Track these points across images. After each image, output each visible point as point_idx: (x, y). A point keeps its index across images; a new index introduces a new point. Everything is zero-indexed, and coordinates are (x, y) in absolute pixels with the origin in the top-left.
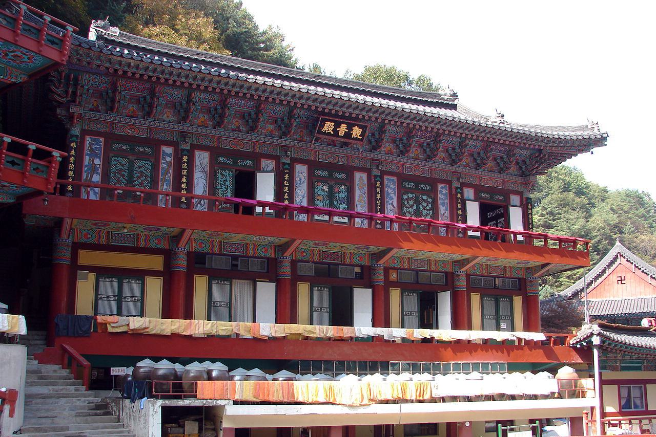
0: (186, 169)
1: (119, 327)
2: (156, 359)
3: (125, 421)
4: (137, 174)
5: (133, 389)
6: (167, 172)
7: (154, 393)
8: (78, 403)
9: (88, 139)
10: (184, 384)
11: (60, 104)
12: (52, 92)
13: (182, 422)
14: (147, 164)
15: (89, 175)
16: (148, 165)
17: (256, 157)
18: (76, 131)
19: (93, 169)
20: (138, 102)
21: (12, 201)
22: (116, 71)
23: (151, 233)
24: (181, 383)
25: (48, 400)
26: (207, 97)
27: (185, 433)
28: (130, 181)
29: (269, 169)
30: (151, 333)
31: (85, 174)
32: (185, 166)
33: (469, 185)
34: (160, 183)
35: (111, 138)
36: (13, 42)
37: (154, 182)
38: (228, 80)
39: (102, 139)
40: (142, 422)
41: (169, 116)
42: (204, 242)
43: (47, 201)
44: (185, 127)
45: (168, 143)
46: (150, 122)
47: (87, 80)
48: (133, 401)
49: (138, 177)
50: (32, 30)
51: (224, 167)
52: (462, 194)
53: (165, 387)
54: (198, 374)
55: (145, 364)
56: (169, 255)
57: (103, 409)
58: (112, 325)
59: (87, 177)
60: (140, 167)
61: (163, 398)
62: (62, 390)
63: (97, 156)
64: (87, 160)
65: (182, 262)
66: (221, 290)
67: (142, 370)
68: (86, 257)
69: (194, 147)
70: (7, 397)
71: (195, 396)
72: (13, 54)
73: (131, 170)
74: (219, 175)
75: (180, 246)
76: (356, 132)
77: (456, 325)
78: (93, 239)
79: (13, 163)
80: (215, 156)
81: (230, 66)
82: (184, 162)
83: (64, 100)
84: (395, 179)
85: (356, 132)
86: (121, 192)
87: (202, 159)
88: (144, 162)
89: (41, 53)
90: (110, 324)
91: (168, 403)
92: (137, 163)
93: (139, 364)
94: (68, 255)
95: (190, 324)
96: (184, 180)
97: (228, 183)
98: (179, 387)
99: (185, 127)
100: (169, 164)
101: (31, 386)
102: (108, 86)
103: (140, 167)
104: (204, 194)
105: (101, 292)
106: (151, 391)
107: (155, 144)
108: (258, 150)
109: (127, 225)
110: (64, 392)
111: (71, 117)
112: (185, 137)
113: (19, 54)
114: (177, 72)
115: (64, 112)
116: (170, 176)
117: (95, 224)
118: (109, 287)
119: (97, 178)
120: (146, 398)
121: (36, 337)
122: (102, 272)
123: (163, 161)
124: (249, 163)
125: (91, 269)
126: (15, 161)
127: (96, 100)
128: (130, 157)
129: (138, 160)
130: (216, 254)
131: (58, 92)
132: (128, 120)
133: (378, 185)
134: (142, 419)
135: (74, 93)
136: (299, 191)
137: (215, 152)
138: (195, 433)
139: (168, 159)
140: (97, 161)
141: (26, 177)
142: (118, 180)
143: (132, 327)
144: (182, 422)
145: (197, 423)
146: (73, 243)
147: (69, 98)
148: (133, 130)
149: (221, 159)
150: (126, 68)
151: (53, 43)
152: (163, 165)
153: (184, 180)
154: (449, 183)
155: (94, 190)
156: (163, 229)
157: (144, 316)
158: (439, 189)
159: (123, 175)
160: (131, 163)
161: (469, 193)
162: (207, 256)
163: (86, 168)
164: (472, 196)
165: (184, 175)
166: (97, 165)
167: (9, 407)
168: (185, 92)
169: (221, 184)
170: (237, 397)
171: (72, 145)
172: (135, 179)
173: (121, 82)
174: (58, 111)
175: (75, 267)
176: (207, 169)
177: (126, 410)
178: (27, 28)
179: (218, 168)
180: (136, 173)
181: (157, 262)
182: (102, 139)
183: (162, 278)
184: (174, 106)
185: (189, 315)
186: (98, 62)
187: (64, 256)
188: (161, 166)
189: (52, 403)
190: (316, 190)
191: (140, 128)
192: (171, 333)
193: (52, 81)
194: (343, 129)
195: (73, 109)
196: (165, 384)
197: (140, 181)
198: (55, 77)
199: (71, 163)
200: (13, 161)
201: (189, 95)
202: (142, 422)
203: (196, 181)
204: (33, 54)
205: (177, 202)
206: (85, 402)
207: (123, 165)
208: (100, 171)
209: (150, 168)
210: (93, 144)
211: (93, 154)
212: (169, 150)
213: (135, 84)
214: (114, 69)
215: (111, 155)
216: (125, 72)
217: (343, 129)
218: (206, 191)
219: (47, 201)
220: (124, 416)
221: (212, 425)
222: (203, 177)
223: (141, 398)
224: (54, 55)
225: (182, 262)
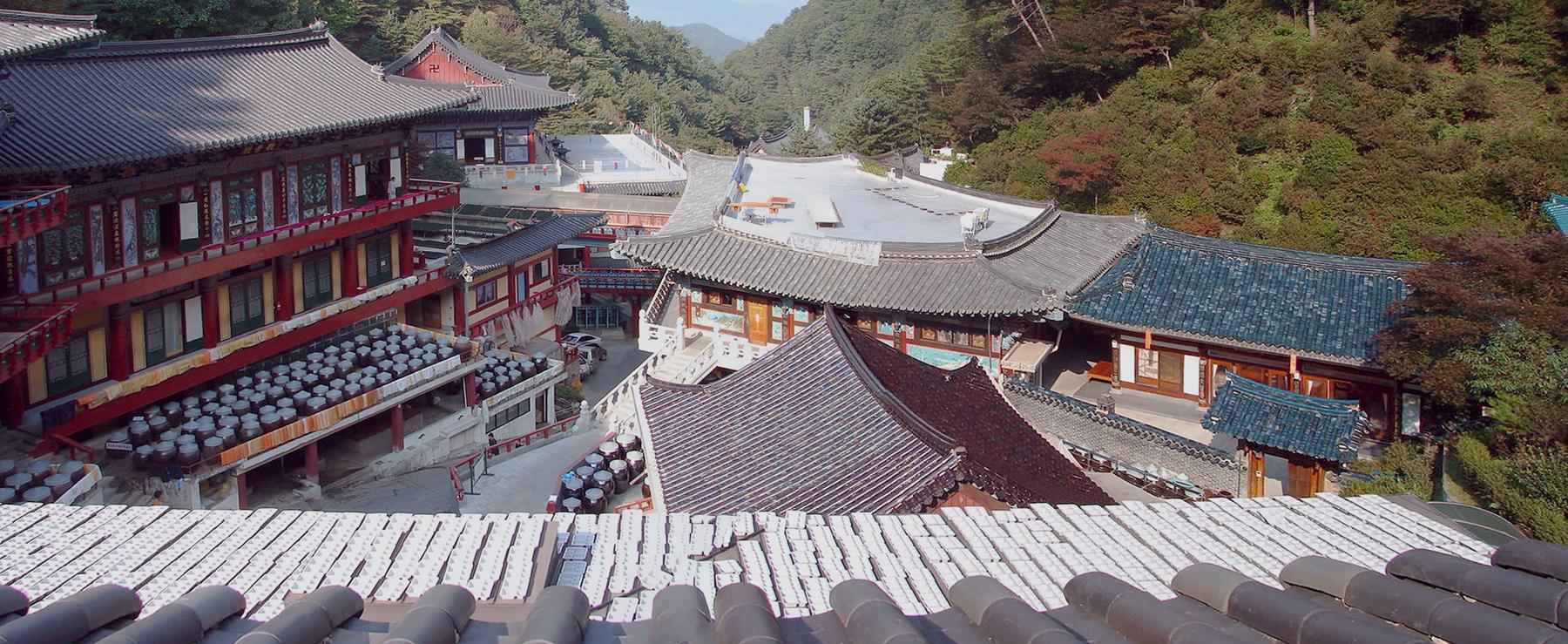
17: (177, 189)
116: (101, 234)
139: (98, 217)
152: (94, 224)
161: (357, 159)
164: (359, 161)
176: (134, 215)
203: (125, 229)
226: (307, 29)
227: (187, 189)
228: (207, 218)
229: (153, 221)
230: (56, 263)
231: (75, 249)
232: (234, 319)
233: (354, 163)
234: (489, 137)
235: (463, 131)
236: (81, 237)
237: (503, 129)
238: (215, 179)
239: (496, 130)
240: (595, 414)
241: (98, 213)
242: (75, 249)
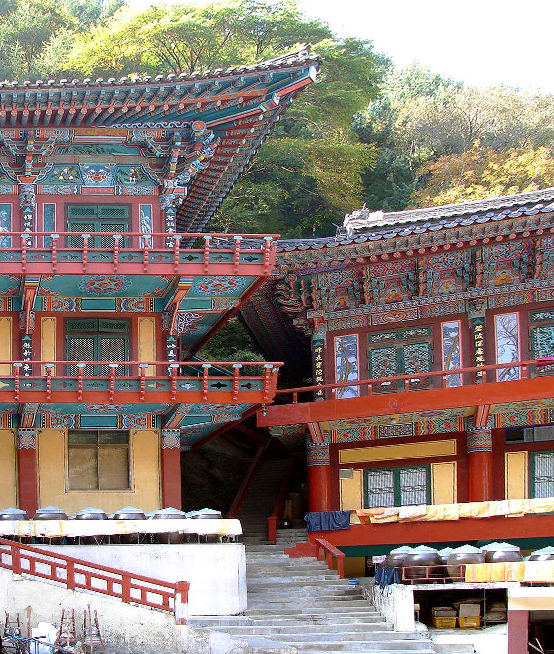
0: (481, 339)
1: (386, 517)
2: (414, 545)
3: (378, 605)
4: (410, 361)
5: (383, 575)
6: (452, 349)
7: (403, 578)
8: (325, 590)
9: (337, 340)
10: (448, 569)
11: (296, 314)
12: (282, 305)
13: (456, 605)
14: (423, 347)
15: (344, 376)
18: (320, 335)
19: (348, 368)
20: (399, 283)
21: (238, 418)
22: (367, 258)
23: (433, 418)
24: (446, 567)
25: (285, 589)
26: (502, 250)
27: (460, 616)
28: (400, 369)
30: (430, 519)
31: (339, 375)
35: (366, 332)
36: (203, 274)
37: (435, 361)
38: (524, 219)
39: (356, 336)
40: (391, 605)
41: (449, 286)
42: (348, 431)
43: (265, 412)
44: (474, 293)
46: (421, 300)
47: (322, 281)
48: (382, 587)
49: (410, 364)
50: (223, 255)
53: (422, 572)
54: (467, 557)
55: (401, 552)
56: (462, 438)
57: (357, 595)
58: (375, 516)
59: (341, 377)
61: (416, 582)
62: (309, 579)
63: (351, 354)
64: (338, 361)
65: (483, 442)
67: (395, 558)
68: (346, 456)
70: (177, 587)
71: (464, 580)
72: (211, 285)
73: (400, 359)
74: (538, 335)
75: (478, 424)
77: (465, 494)
78: (356, 437)
79: (219, 385)
80: (529, 314)
81: (394, 225)
82: (478, 333)
83: (300, 309)
86: (389, 383)
88: (418, 345)
89: (238, 274)
90: (373, 516)
91: (422, 587)
92: (407, 350)
93: (392, 552)
94: (327, 457)
95: (489, 505)
96: (479, 352)
98: (440, 571)
99: (474, 293)
100: (455, 340)
101: (273, 576)
102: (352, 279)
104: (515, 361)
105: (371, 485)
106: (400, 576)
107: (433, 323)
109: (396, 416)
110: (312, 580)
111: (311, 323)
112: (474, 305)
113: (217, 282)
114: (439, 234)
115: (302, 321)
117: (353, 422)
118: (382, 481)
119: (353, 376)
120: (395, 584)
121: (299, 534)
122: (369, 467)
123: (445, 339)
125: (356, 466)
126: (221, 383)
127: (341, 298)
128: (397, 346)
129: (408, 345)
130: (539, 426)
131: (290, 304)
132: (388, 307)
134: (390, 603)
135: (310, 299)
138: (474, 615)
140: (352, 359)
141: (235, 395)
142: (383, 373)
143: (402, 516)
144: (456, 605)
145: (478, 606)
146: (331, 445)
147: (305, 306)
148: (397, 316)
150: (366, 253)
151: (250, 259)
152: (445, 342)
153: (479, 352)
155: (352, 389)
156: (448, 411)
157: (433, 503)
160: (400, 351)
162: (525, 430)
163: (338, 370)
165: (479, 347)
166: (353, 363)
167: (180, 595)
168: (466, 253)
169: (541, 344)
170: (527, 579)
171: (316, 351)
172: (406, 367)
173: (367, 272)
174: (295, 322)
175: (335, 468)
177: (378, 595)
178: (217, 255)
179: (534, 327)
180: (407, 360)
181: (449, 447)
182: (356, 336)
183: (455, 463)
184: (454, 274)
185: (498, 493)
186: (328, 259)
187: (320, 458)
189: (291, 591)
191: (409, 310)
192: (459, 518)
193: (279, 295)
195: (310, 315)
196: (422, 570)
197: (414, 367)
198: (282, 290)
199: (318, 369)
200: (219, 383)
201: (474, 256)
202: (391, 605)
204: (232, 278)
205: (471, 378)
206: (334, 589)
208: (357, 368)
210: (345, 343)
211: (345, 353)
212: (455, 324)
213: (389, 265)
214: (401, 252)
215: (370, 349)
216: (367, 258)
218: (517, 358)
219: (265, 412)
220: (376, 601)
221: (502, 607)
222: (511, 343)
223: (392, 582)
224: (255, 271)
225: (483, 442)
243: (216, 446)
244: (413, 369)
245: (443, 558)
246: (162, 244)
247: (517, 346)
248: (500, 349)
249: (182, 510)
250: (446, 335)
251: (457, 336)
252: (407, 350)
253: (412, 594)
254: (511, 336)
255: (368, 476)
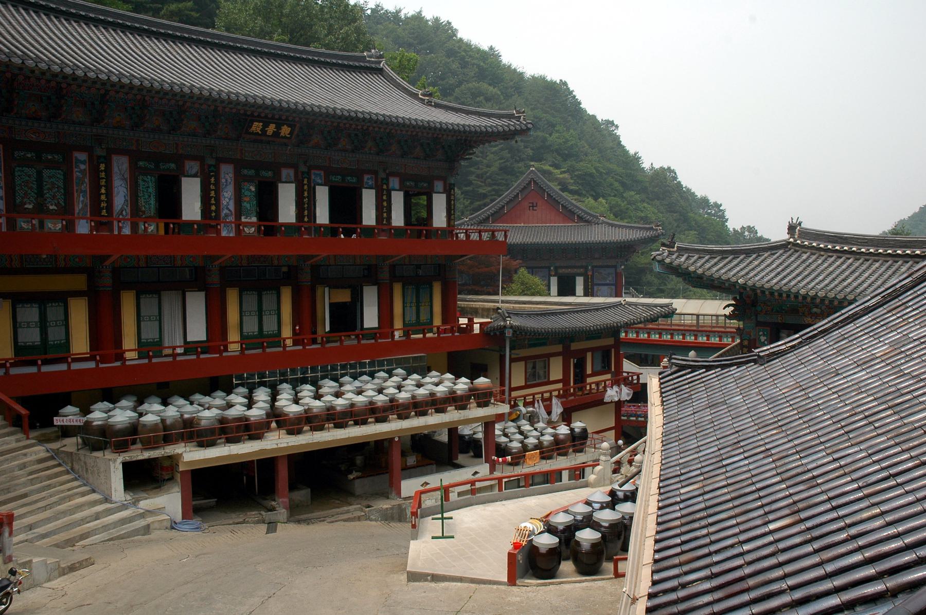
16: (60, 174)
17: (180, 159)
28: (40, 193)
29: (194, 171)
32: (103, 175)
33: (318, 168)
34: (76, 195)
45: (82, 149)
49: (49, 189)
51: (249, 180)
52: (388, 185)
60: (50, 177)
66: (149, 305)
69: (221, 160)
76: (285, 130)
84: (322, 173)
85: (285, 130)
87: (121, 165)
92: (46, 173)
96: (103, 191)
97: (151, 190)
103: (50, 177)
108: (181, 152)
116: (86, 186)
118: (30, 314)
124: (173, 166)
133: (305, 182)
136: (225, 193)
137: (135, 157)
139: (83, 167)
149: (141, 163)
152: (77, 174)
153: (103, 191)
154: (375, 173)
158: (365, 180)
159: (31, 188)
160: (39, 174)
161: (394, 182)
164: (397, 186)
176: (127, 176)
181: (80, 282)
188: (75, 176)
190: (243, 191)
194: (271, 129)
203: (115, 190)
207: (29, 176)
209: (62, 177)
212: (83, 156)
217: (271, 129)
225: (107, 281)
226: (361, 54)
227: (192, 163)
228: (213, 201)
229: (151, 190)
230: (30, 206)
231: (54, 197)
232: (245, 330)
233: (391, 185)
234: (580, 275)
235: (556, 268)
236: (61, 184)
237: (593, 267)
238: (227, 161)
239: (586, 268)
240: (619, 463)
241: (84, 162)
242: (54, 197)
243: (628, 494)
244: (51, 195)
245: (252, 419)
246: (105, 224)
247: (127, 189)
248: (116, 189)
249: (161, 405)
250: (77, 167)
251: (85, 169)
252: (46, 173)
253: (121, 467)
254: (124, 179)
255: (66, 339)
